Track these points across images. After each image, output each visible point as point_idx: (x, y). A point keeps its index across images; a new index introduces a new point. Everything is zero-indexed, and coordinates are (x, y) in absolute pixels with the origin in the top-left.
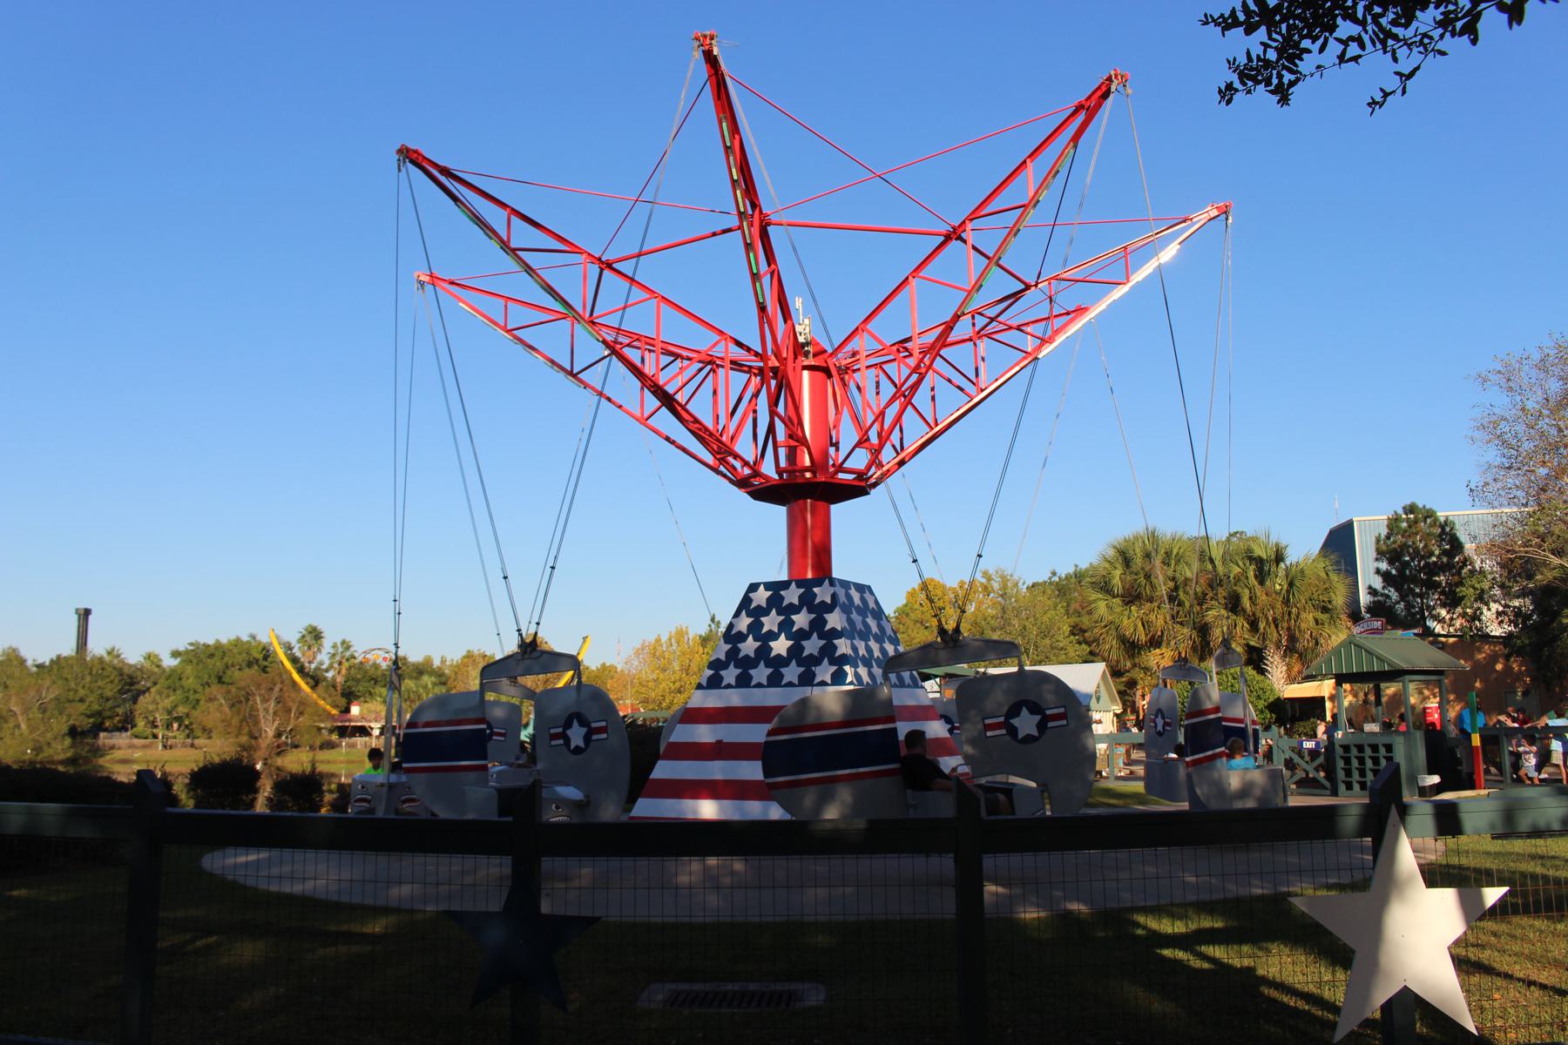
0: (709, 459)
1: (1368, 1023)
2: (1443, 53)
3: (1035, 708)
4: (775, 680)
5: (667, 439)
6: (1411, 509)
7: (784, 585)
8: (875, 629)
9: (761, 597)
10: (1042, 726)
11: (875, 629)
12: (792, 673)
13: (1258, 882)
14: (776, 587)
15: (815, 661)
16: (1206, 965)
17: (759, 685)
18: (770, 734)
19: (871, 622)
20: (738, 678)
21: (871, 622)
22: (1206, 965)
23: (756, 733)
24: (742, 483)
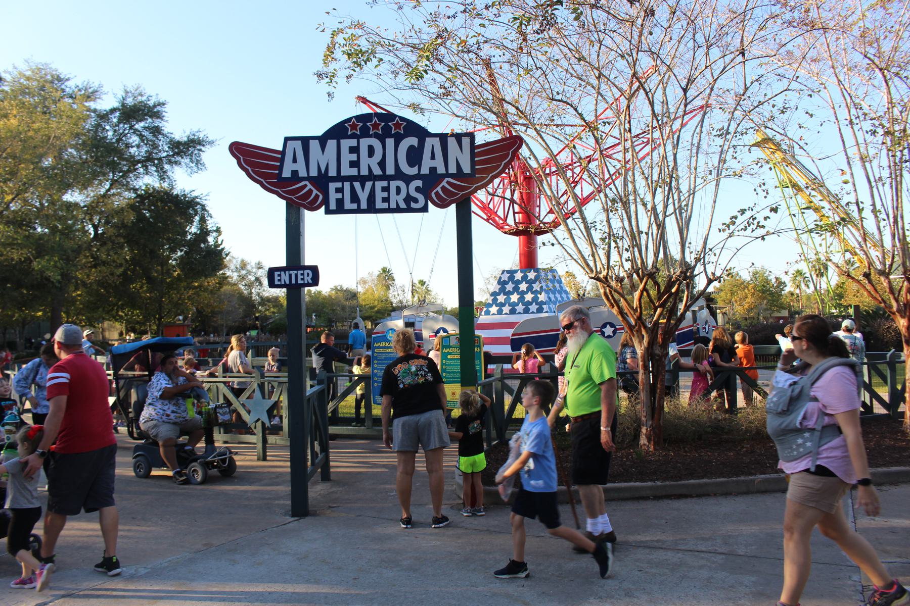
0: (485, 217)
1: (777, 460)
2: (364, 100)
3: (612, 325)
4: (513, 312)
5: (843, 141)
6: (314, 270)
7: (516, 271)
8: (558, 288)
9: (505, 277)
10: (614, 332)
11: (558, 288)
12: (533, 308)
13: (775, 399)
14: (512, 273)
15: (502, 305)
16: (506, 408)
17: (519, 313)
18: (513, 335)
19: (557, 285)
20: (510, 310)
21: (557, 285)
22: (506, 408)
23: (508, 333)
24: (500, 227)
